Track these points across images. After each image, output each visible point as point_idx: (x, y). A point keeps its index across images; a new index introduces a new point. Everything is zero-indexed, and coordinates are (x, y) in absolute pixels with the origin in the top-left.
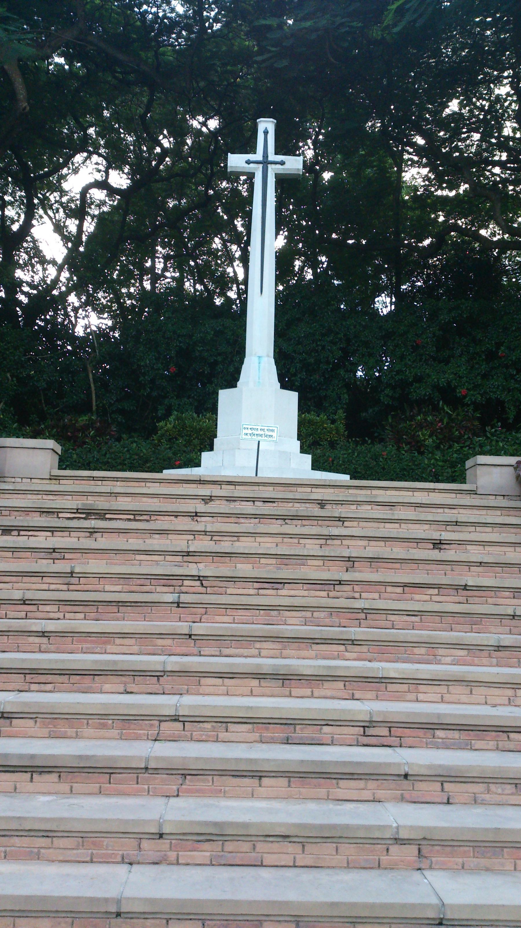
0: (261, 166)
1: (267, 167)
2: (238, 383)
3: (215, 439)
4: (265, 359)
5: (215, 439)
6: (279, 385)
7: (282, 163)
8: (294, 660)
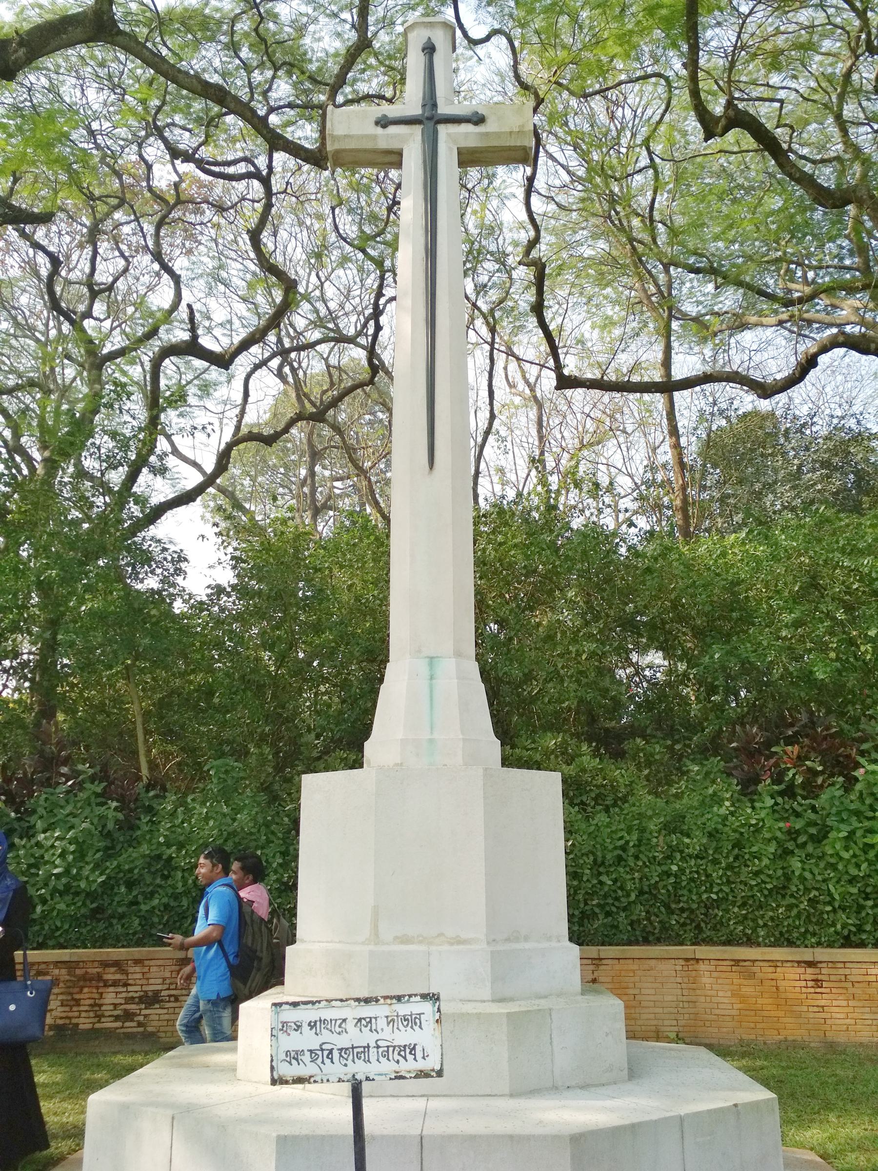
0: (417, 130)
1: (435, 133)
2: (367, 745)
3: (288, 949)
4: (448, 666)
5: (288, 949)
6: (494, 747)
7: (384, 122)
8: (806, 1151)
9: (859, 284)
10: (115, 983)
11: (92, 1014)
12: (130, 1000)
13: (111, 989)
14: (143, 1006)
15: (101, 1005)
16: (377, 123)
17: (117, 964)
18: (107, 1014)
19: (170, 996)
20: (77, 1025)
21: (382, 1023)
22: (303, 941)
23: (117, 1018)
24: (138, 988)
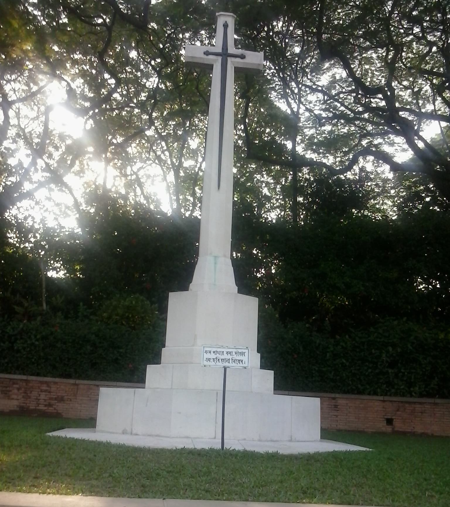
0: (220, 58)
9: (52, 383)
10: (45, 391)
11: (35, 403)
12: (51, 399)
13: (44, 393)
14: (56, 402)
15: (39, 400)
16: (204, 53)
17: (46, 383)
18: (42, 403)
19: (68, 399)
20: (29, 406)
21: (234, 353)
22: (167, 347)
23: (46, 406)
24: (54, 394)
